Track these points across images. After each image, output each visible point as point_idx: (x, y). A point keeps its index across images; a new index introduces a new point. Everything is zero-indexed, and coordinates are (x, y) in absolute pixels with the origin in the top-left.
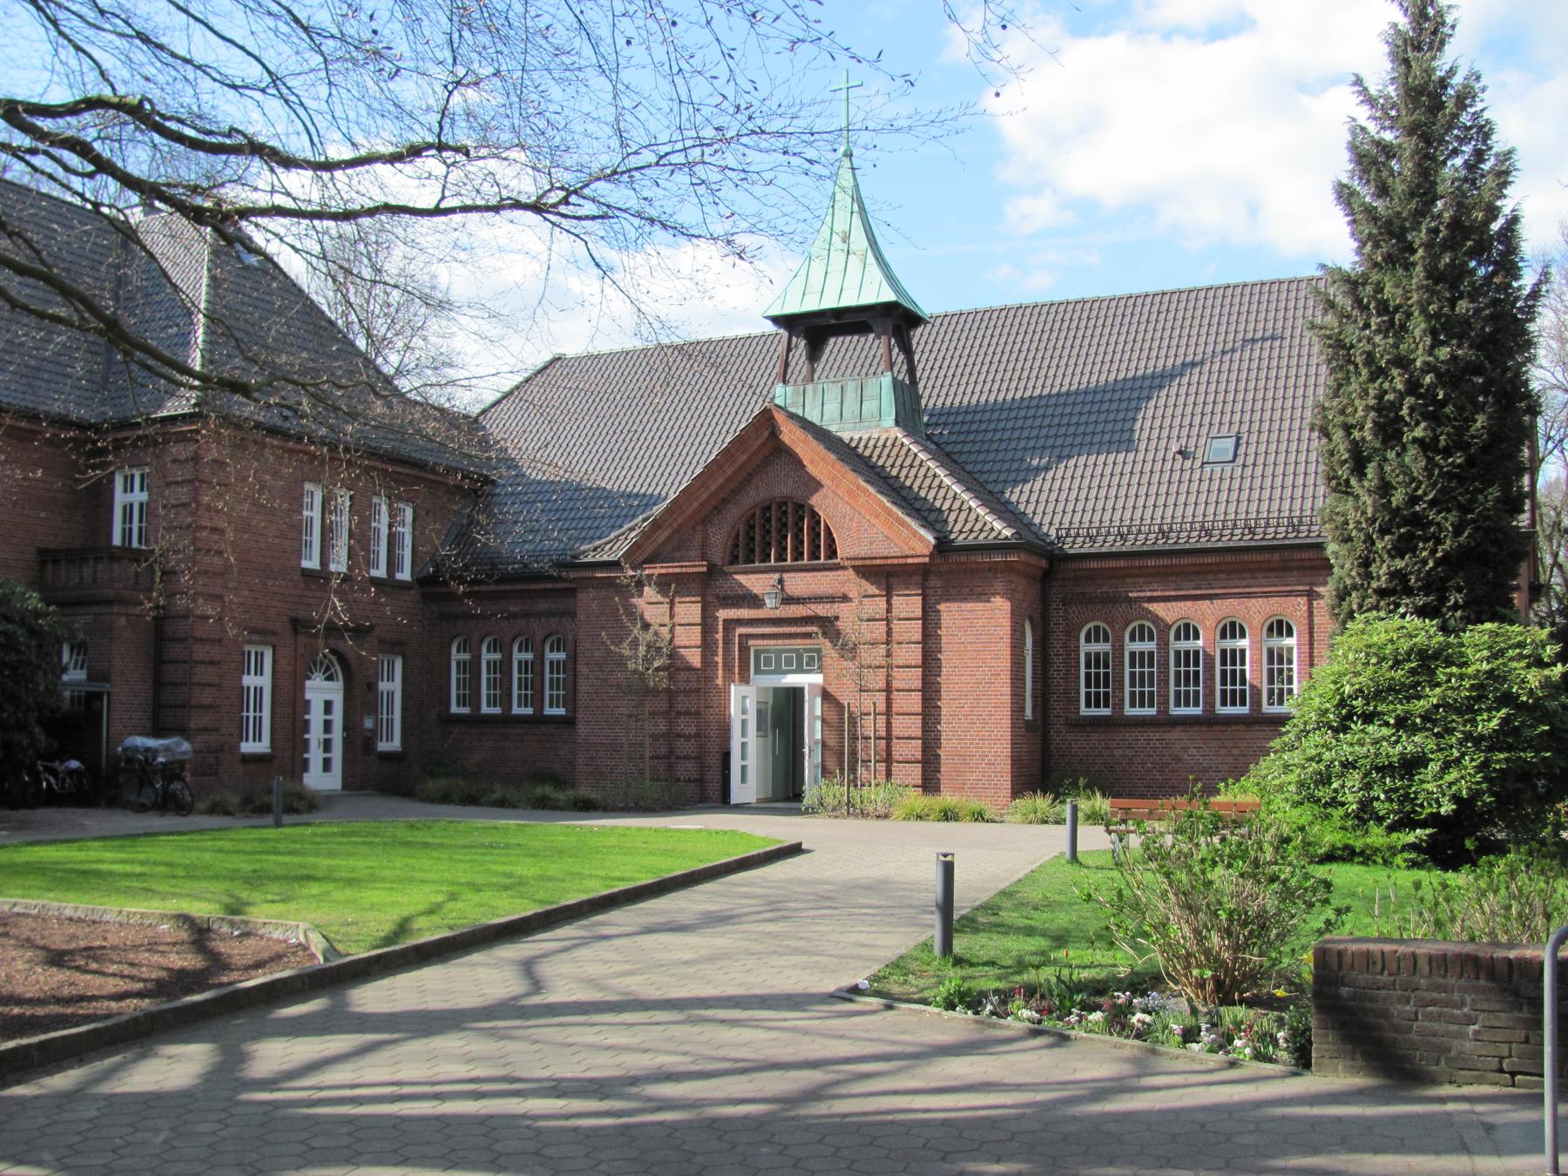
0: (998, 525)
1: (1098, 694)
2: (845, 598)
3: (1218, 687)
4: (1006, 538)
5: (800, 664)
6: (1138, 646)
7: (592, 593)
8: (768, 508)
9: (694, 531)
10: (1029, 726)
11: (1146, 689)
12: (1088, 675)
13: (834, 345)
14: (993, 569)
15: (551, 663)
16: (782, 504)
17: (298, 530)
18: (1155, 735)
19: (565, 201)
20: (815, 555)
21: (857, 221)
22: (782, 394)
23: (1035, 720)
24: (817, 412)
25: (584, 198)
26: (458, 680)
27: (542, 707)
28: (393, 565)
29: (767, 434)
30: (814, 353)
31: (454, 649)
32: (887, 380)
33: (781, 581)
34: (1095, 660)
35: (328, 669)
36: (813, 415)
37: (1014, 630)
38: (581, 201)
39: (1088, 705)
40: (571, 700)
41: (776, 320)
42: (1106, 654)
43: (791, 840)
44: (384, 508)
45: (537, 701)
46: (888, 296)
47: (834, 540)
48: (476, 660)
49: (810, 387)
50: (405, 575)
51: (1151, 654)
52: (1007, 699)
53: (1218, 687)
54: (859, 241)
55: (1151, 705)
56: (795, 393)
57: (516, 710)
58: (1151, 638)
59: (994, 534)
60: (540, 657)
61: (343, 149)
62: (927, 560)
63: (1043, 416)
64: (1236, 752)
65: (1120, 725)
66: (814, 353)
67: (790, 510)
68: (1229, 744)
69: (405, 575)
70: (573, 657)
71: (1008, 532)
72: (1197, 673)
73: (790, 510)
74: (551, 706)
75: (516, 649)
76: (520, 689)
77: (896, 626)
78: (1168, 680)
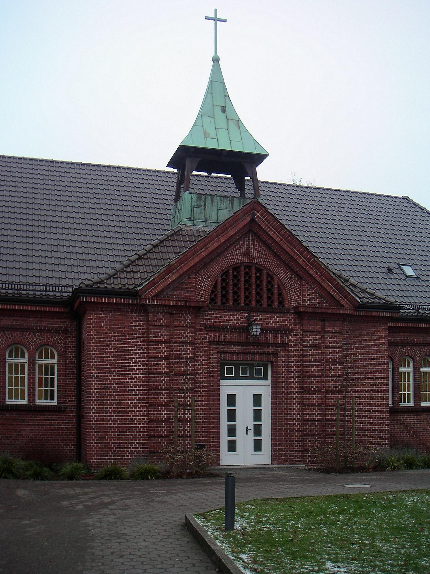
29: (249, 219)
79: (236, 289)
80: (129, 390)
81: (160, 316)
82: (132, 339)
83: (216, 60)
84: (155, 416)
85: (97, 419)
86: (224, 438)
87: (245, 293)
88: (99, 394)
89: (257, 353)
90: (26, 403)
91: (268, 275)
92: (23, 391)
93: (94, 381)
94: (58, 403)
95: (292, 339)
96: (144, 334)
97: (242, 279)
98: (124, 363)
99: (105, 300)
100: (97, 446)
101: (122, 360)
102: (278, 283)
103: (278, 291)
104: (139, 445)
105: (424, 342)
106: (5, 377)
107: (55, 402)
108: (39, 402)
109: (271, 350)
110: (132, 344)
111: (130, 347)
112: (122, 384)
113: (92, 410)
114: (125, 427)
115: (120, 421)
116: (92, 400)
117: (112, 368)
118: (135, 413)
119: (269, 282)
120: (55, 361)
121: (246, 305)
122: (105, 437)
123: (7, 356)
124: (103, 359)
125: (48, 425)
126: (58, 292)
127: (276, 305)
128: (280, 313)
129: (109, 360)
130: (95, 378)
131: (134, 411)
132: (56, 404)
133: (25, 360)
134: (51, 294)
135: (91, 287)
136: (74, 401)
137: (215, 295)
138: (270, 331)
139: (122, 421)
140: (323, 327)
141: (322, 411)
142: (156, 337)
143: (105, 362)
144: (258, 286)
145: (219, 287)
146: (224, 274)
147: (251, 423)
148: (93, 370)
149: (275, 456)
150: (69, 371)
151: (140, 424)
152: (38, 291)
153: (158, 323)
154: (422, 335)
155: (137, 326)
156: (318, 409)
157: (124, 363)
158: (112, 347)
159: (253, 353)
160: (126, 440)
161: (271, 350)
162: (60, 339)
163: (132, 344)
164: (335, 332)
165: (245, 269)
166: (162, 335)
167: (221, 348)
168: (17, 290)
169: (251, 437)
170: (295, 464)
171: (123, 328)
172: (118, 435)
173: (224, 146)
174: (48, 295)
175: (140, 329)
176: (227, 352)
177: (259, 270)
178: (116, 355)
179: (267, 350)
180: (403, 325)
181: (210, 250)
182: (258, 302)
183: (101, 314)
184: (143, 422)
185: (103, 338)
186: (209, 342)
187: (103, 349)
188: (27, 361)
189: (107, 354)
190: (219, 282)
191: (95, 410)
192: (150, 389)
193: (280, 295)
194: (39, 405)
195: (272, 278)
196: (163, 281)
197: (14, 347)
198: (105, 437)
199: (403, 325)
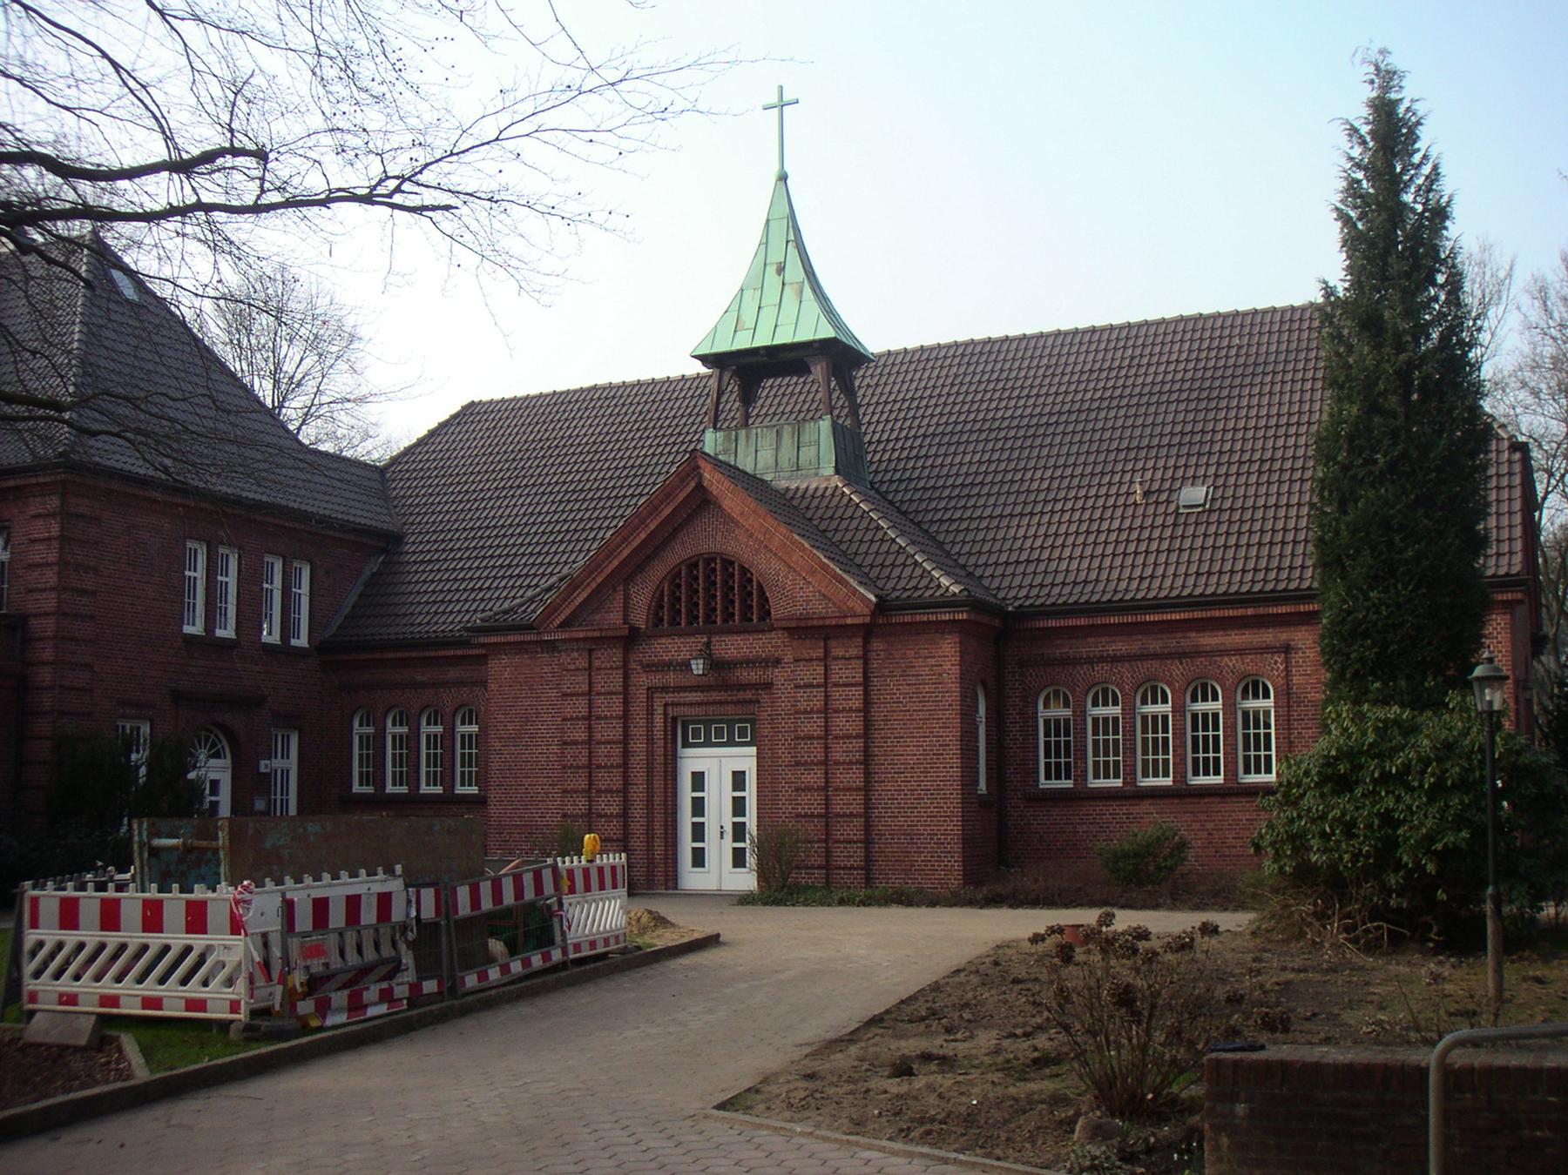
0: (945, 581)
1: (1106, 763)
2: (777, 662)
3: (1241, 753)
4: (954, 594)
5: (708, 735)
6: (1101, 711)
7: (505, 660)
8: (696, 565)
9: (615, 591)
10: (984, 802)
11: (1111, 759)
12: (1047, 744)
13: (769, 388)
14: (940, 627)
15: (463, 736)
16: (710, 559)
17: (178, 592)
18: (1121, 810)
19: (398, 190)
20: (746, 618)
21: (792, 252)
22: (711, 442)
23: (989, 794)
24: (750, 459)
25: (419, 185)
26: (361, 756)
27: (453, 786)
28: (287, 629)
29: (693, 484)
30: (748, 398)
31: (356, 724)
32: (825, 425)
33: (708, 644)
34: (1054, 726)
35: (214, 745)
36: (746, 463)
37: (963, 696)
38: (416, 189)
39: (1048, 777)
40: (482, 780)
41: (704, 359)
42: (1067, 721)
43: (709, 930)
44: (278, 566)
45: (447, 779)
46: (827, 332)
47: (767, 600)
48: (380, 735)
49: (743, 433)
50: (302, 641)
51: (1116, 720)
52: (956, 772)
53: (1241, 753)
54: (795, 272)
55: (1117, 776)
56: (727, 439)
57: (424, 789)
58: (1115, 703)
59: (941, 591)
60: (450, 732)
61: (140, 134)
62: (868, 620)
63: (999, 460)
64: (1210, 826)
65: (1080, 799)
66: (748, 398)
67: (718, 567)
68: (1202, 817)
69: (302, 641)
70: (484, 730)
71: (955, 589)
72: (1165, 740)
73: (718, 567)
74: (463, 784)
75: (424, 721)
76: (428, 765)
77: (836, 693)
78: (1135, 749)
81: (576, 654)
83: (783, 178)
84: (569, 809)
86: (687, 845)
89: (727, 703)
95: (778, 675)
105: (1145, 652)
107: (1220, 779)
109: (749, 695)
123: (458, 722)
138: (741, 664)
140: (827, 652)
147: (728, 820)
149: (762, 876)
153: (572, 667)
154: (1140, 637)
159: (720, 703)
161: (749, 695)
164: (850, 658)
167: (669, 698)
169: (728, 844)
176: (678, 704)
179: (741, 695)
180: (1083, 622)
181: (635, 544)
186: (648, 689)
192: (564, 767)
199: (1083, 622)
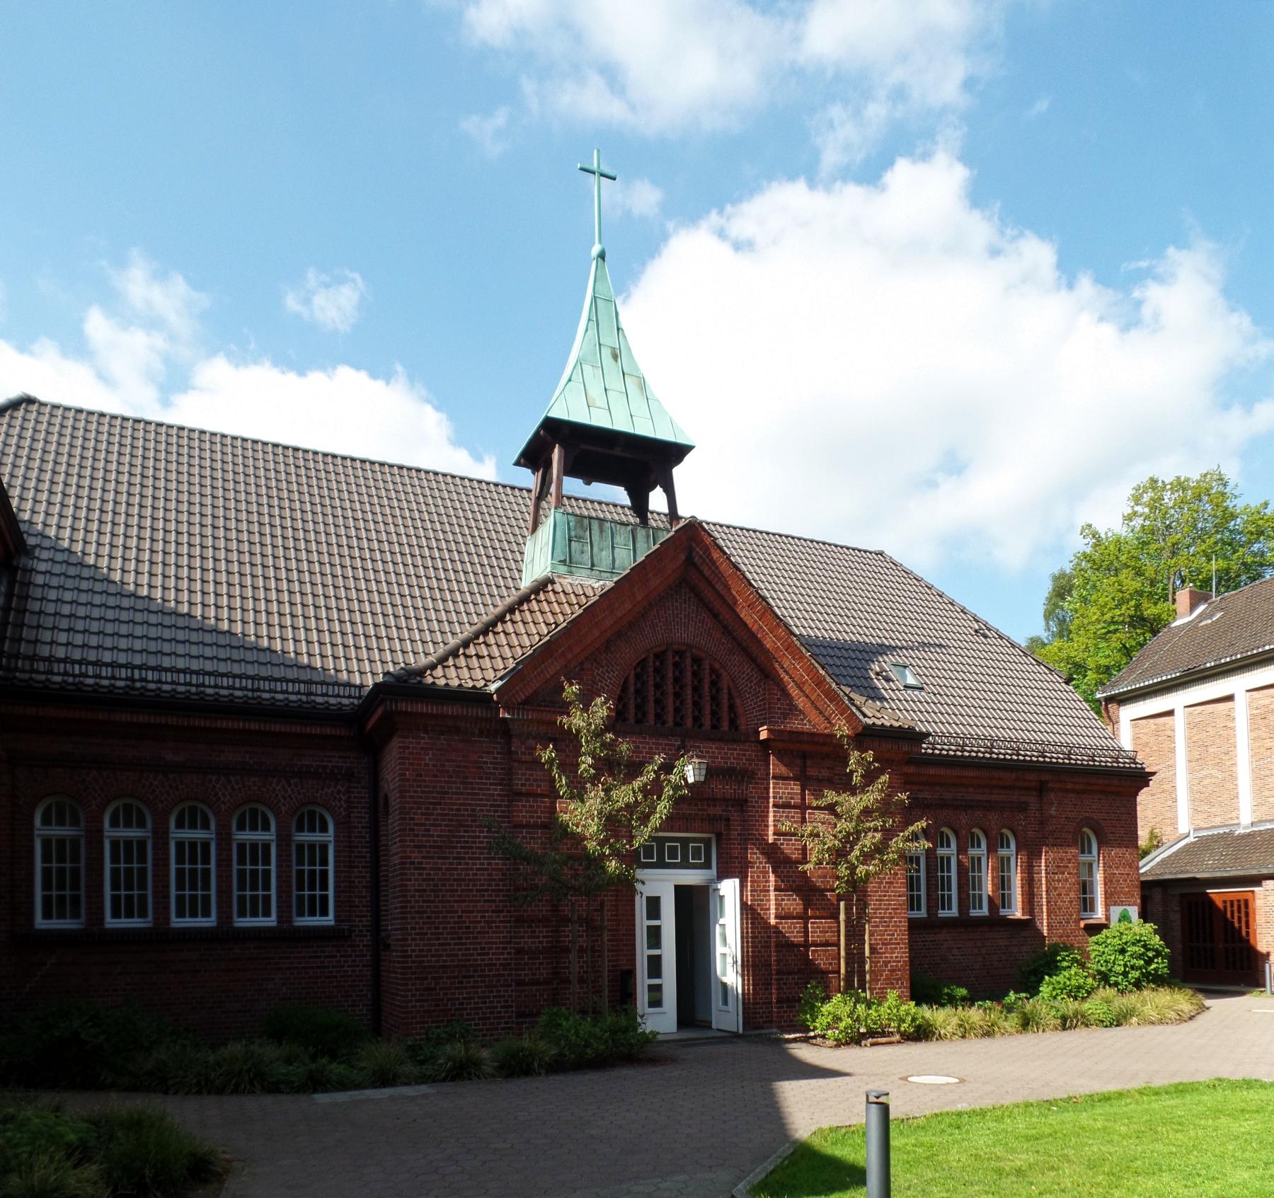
29: (683, 557)
79: (658, 695)
80: (477, 891)
82: (481, 789)
85: (420, 951)
87: (674, 702)
88: (424, 901)
90: (275, 924)
91: (712, 670)
92: (267, 899)
93: (414, 874)
94: (336, 921)
96: (504, 779)
97: (670, 674)
98: (469, 837)
99: (432, 709)
100: (421, 1006)
101: (465, 831)
102: (729, 687)
103: (729, 699)
104: (498, 1002)
106: (231, 871)
107: (329, 920)
108: (177, 922)
109: (718, 810)
110: (482, 800)
111: (479, 805)
112: (465, 880)
113: (411, 934)
114: (471, 965)
115: (463, 955)
116: (410, 912)
117: (447, 847)
118: (489, 938)
119: (713, 683)
120: (329, 836)
121: (677, 724)
122: (435, 989)
124: (429, 830)
125: (318, 967)
126: (333, 696)
127: (725, 726)
128: (734, 741)
129: (441, 831)
130: (416, 869)
131: (488, 933)
132: (332, 923)
133: (270, 836)
134: (320, 700)
135: (405, 681)
136: (366, 916)
137: (624, 706)
139: (466, 955)
141: (552, 931)
142: (525, 785)
143: (433, 836)
144: (695, 689)
145: (632, 689)
146: (638, 664)
148: (411, 852)
150: (356, 857)
151: (499, 959)
152: (293, 693)
155: (491, 763)
156: (544, 927)
157: (469, 837)
158: (445, 804)
160: (474, 993)
161: (718, 810)
162: (339, 792)
163: (482, 800)
165: (674, 657)
166: (536, 780)
168: (253, 690)
170: (762, 1028)
171: (464, 767)
172: (459, 982)
173: (621, 424)
174: (314, 701)
175: (497, 769)
177: (697, 660)
178: (452, 820)
182: (696, 719)
183: (424, 738)
184: (503, 954)
185: (428, 787)
187: (429, 809)
188: (274, 838)
189: (437, 820)
190: (632, 681)
191: (416, 934)
193: (732, 707)
194: (113, 930)
195: (718, 676)
196: (539, 674)
197: (247, 808)
198: (435, 989)
